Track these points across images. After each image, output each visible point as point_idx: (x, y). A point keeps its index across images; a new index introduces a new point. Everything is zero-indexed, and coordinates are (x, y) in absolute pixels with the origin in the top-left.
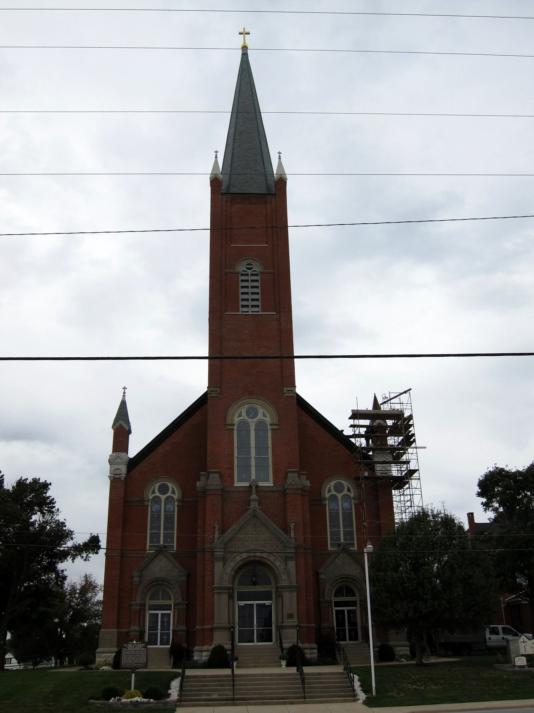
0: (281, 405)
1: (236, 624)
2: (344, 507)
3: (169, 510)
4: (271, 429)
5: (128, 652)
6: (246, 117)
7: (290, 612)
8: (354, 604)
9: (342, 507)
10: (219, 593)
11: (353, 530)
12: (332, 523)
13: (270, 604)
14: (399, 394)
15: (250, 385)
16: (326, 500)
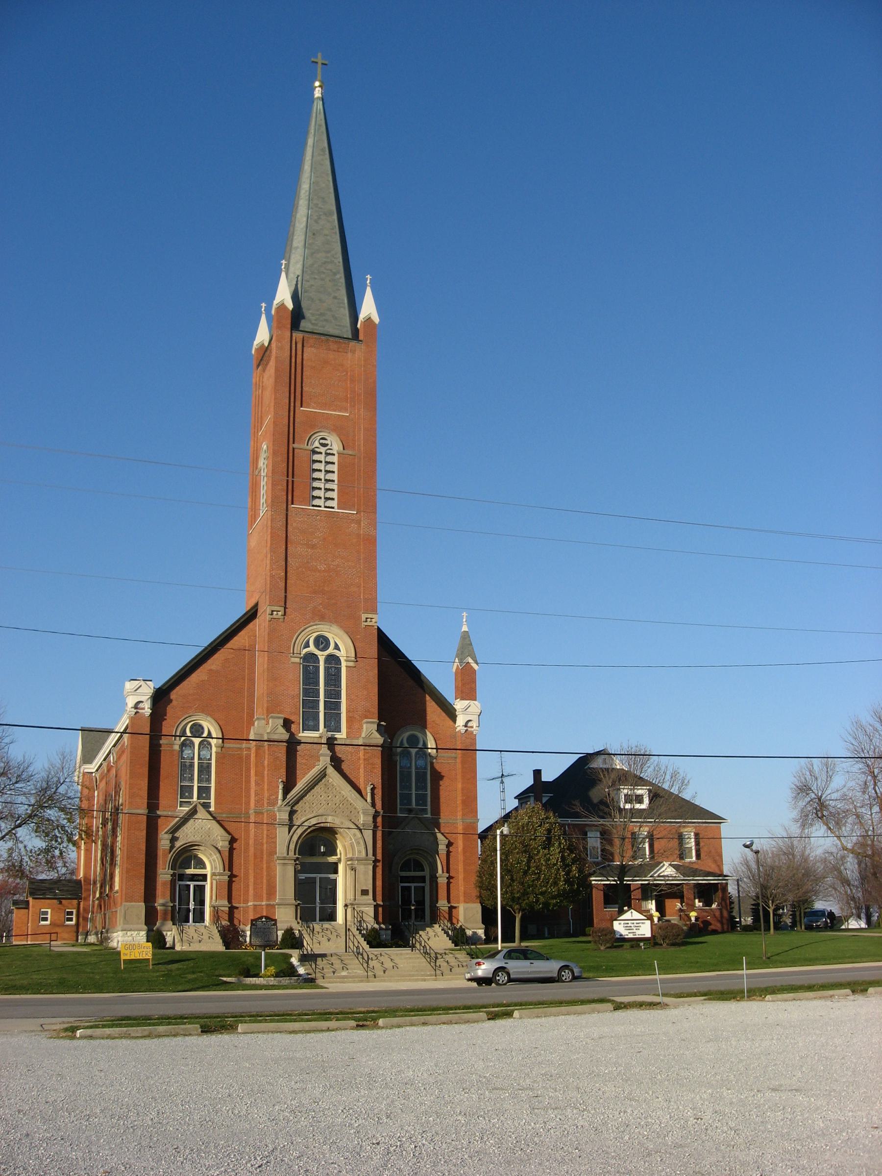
6: (321, 208)
7: (364, 888)
8: (422, 879)
16: (397, 755)
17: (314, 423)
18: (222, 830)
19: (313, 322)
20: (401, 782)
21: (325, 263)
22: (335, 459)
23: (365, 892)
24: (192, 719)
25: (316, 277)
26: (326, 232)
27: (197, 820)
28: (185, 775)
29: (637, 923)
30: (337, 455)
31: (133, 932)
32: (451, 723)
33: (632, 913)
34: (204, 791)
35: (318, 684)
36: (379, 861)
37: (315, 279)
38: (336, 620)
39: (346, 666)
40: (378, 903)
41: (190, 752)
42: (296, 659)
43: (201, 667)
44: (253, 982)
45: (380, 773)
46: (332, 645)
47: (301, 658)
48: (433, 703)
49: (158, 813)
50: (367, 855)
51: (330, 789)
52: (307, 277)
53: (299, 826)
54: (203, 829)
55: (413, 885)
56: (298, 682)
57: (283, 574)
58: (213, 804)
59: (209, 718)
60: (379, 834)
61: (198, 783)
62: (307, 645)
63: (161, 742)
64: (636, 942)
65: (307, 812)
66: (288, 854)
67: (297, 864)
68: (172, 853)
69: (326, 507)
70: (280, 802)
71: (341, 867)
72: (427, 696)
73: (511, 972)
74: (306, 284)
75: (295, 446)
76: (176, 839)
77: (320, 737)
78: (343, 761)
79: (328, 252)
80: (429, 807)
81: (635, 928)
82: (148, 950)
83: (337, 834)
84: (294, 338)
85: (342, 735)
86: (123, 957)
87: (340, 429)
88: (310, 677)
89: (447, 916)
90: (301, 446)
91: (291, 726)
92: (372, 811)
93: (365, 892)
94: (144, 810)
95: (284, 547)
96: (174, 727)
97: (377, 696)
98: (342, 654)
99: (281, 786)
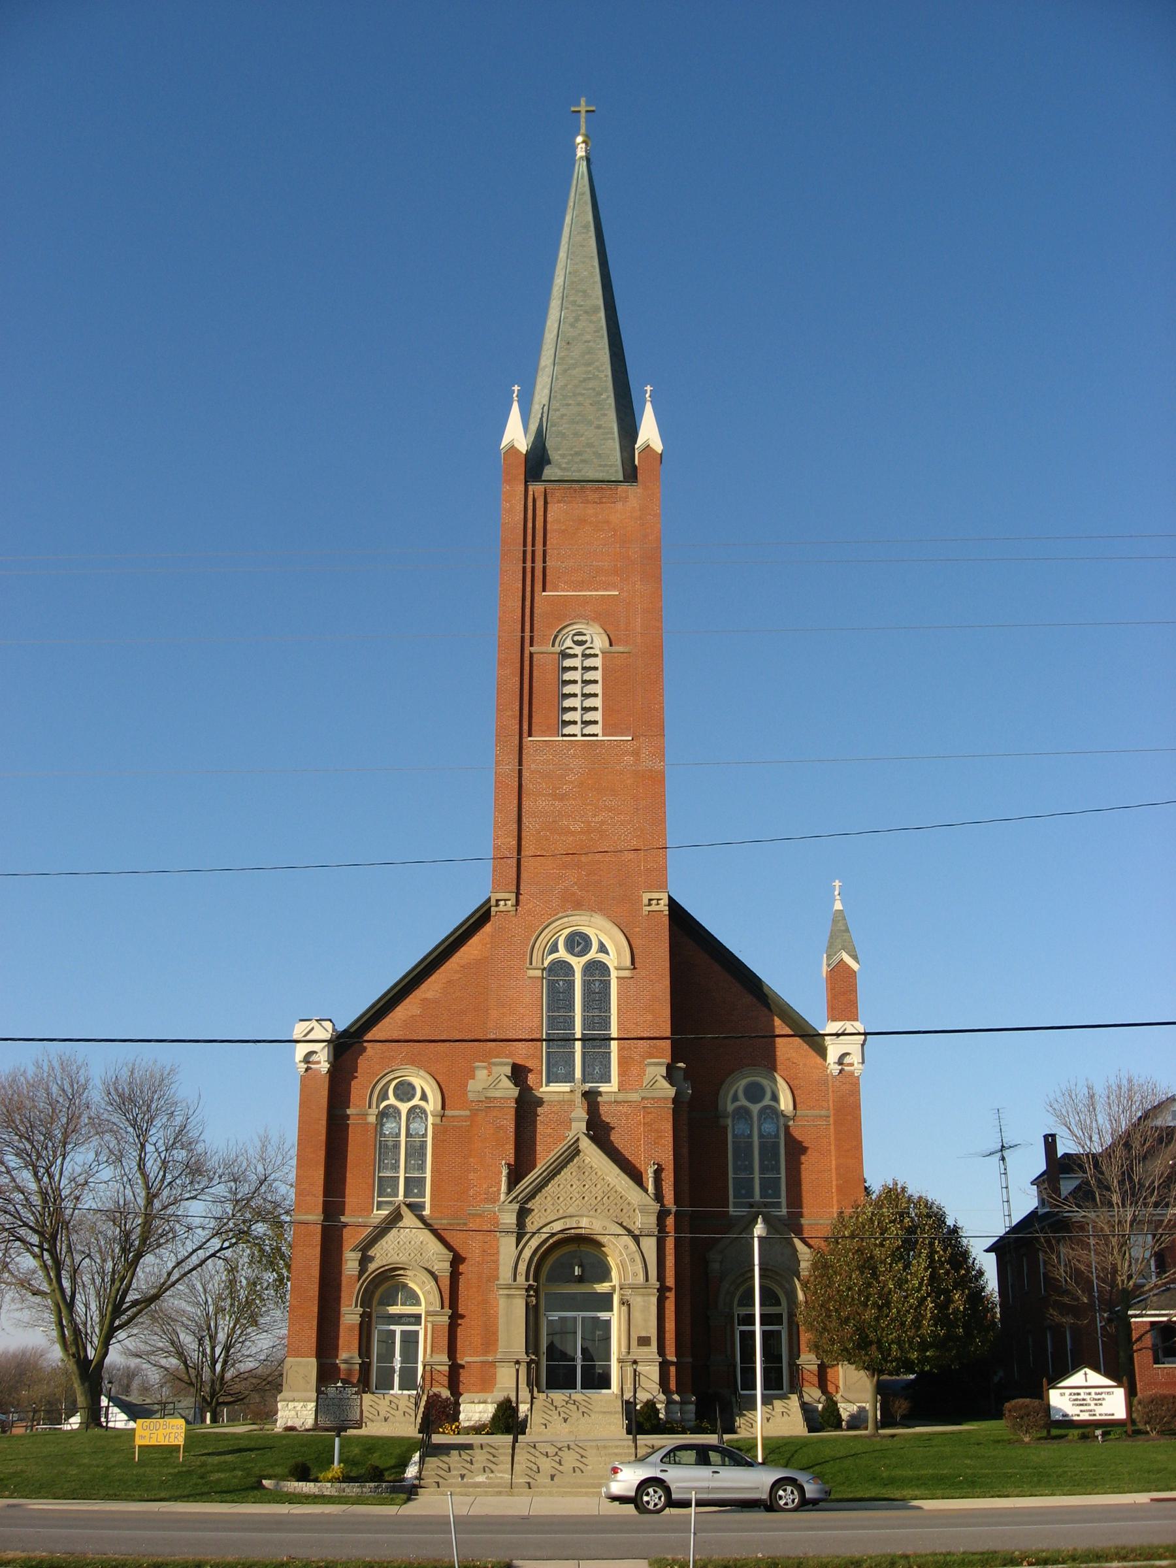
1: (541, 1353)
3: (417, 1134)
5: (328, 1400)
6: (581, 306)
7: (643, 1334)
11: (780, 1178)
14: (548, 1235)
15: (576, 887)
16: (728, 1117)
17: (565, 612)
18: (439, 1244)
19: (564, 466)
21: (585, 380)
22: (597, 662)
23: (644, 1341)
24: (396, 1075)
25: (570, 402)
26: (588, 337)
27: (402, 1230)
28: (386, 1161)
29: (1096, 1394)
30: (600, 655)
31: (296, 1404)
32: (819, 1060)
33: (1086, 1374)
34: (414, 1184)
35: (571, 1007)
36: (669, 1289)
37: (570, 405)
38: (600, 907)
39: (617, 978)
40: (669, 1358)
41: (394, 1125)
42: (537, 971)
44: (298, 1490)
45: (671, 1145)
47: (544, 969)
49: (343, 1219)
50: (647, 1280)
51: (586, 1174)
52: (555, 404)
53: (534, 1233)
54: (413, 1243)
56: (539, 1007)
57: (515, 843)
58: (428, 1206)
59: (422, 1073)
60: (670, 1244)
61: (405, 1173)
62: (554, 949)
63: (349, 1112)
64: (1086, 1429)
65: (549, 1211)
66: (515, 1280)
67: (532, 1296)
68: (361, 1281)
69: (583, 735)
70: (502, 1197)
72: (776, 1018)
73: (673, 1487)
74: (554, 416)
75: (533, 649)
76: (371, 1259)
77: (571, 1091)
78: (614, 1128)
79: (589, 364)
80: (783, 1200)
81: (1093, 1403)
82: (179, 1431)
84: (531, 493)
85: (610, 1088)
86: (139, 1442)
87: (603, 616)
88: (560, 998)
89: (815, 1380)
90: (543, 649)
91: (527, 1077)
93: (644, 1341)
94: (316, 1216)
95: (516, 802)
96: (367, 1088)
97: (669, 1022)
98: (611, 961)
99: (505, 1172)
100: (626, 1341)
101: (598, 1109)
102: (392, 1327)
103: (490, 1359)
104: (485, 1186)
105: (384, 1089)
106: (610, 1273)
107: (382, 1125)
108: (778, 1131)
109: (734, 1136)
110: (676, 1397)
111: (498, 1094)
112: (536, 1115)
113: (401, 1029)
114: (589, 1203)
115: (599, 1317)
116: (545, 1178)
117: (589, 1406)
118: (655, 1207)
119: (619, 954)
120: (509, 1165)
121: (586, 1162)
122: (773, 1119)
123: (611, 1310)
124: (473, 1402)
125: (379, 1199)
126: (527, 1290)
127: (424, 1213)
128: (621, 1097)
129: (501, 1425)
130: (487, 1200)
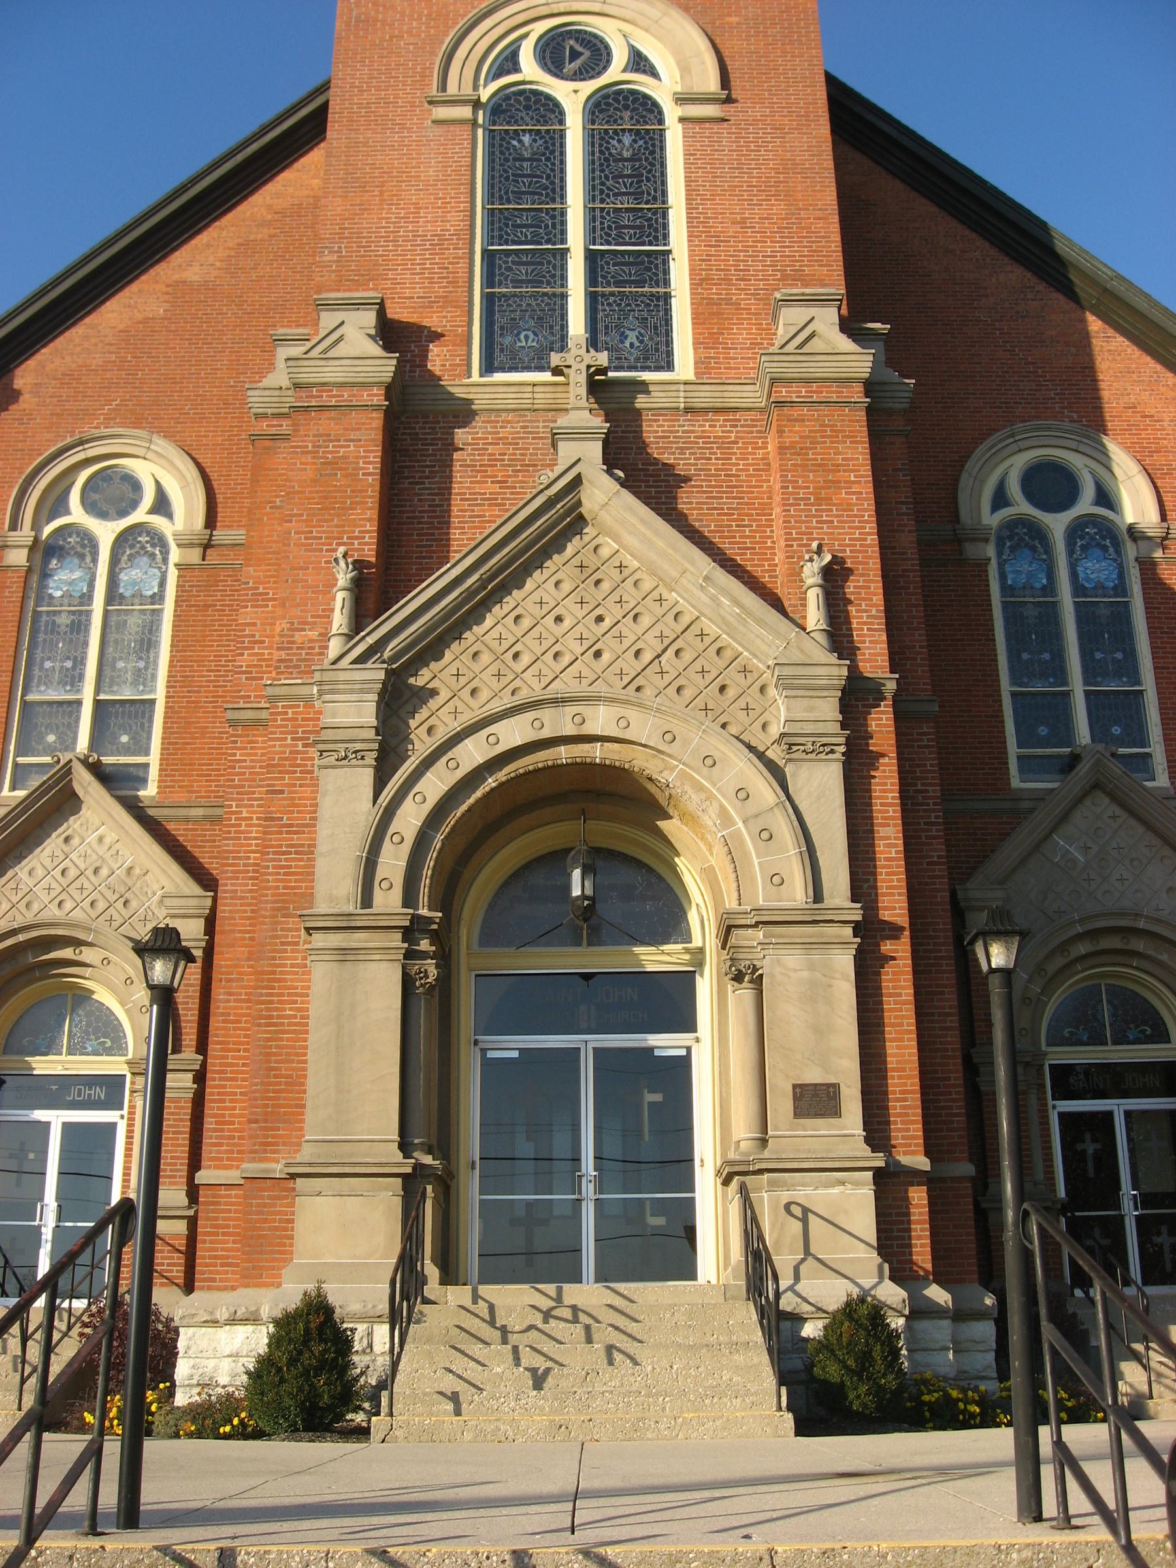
0: (734, 19)
2: (1081, 575)
3: (139, 595)
4: (682, 120)
7: (814, 1076)
9: (1074, 575)
10: (345, 954)
12: (1025, 656)
13: (683, 1052)
16: (987, 541)
20: (1013, 655)
24: (91, 453)
35: (557, 190)
36: (894, 931)
40: (905, 1160)
41: (77, 574)
43: (144, 278)
45: (869, 505)
46: (620, 57)
48: (1120, 341)
50: (818, 897)
54: (104, 872)
55: (1118, 1107)
58: (154, 773)
59: (161, 445)
62: (509, 62)
66: (367, 900)
67: (424, 955)
70: (335, 647)
71: (705, 989)
72: (1090, 318)
78: (687, 479)
83: (668, 817)
92: (836, 671)
97: (836, 219)
98: (662, 91)
99: (343, 576)
100: (754, 1105)
101: (638, 433)
102: (40, 1115)
103: (278, 1169)
104: (281, 625)
105: (57, 491)
106: (685, 914)
107: (45, 575)
108: (1121, 576)
109: (1006, 589)
110: (938, 1294)
111: (331, 373)
112: (450, 447)
113: (113, 349)
114: (615, 668)
115: (651, 1049)
116: (471, 593)
117: (632, 1327)
118: (835, 671)
119: (685, 69)
120: (359, 565)
121: (605, 552)
122: (1105, 548)
123: (687, 1023)
124: (214, 1323)
125: (20, 760)
126: (409, 934)
127: (141, 793)
128: (704, 397)
129: (287, 1401)
130: (286, 666)
